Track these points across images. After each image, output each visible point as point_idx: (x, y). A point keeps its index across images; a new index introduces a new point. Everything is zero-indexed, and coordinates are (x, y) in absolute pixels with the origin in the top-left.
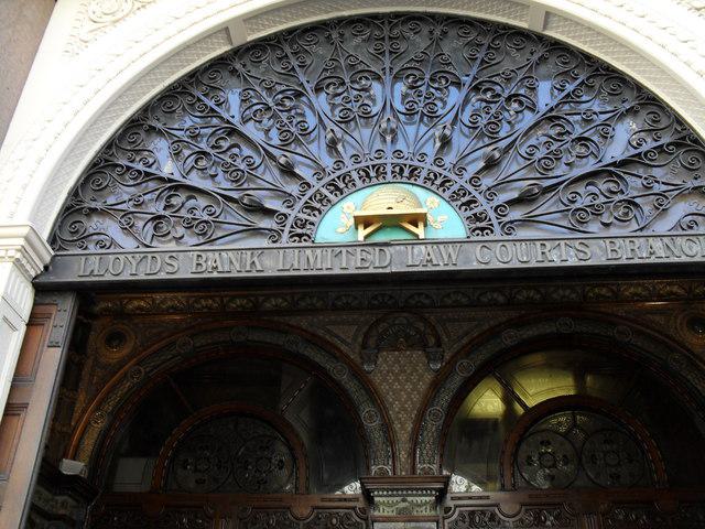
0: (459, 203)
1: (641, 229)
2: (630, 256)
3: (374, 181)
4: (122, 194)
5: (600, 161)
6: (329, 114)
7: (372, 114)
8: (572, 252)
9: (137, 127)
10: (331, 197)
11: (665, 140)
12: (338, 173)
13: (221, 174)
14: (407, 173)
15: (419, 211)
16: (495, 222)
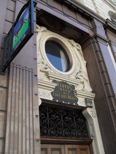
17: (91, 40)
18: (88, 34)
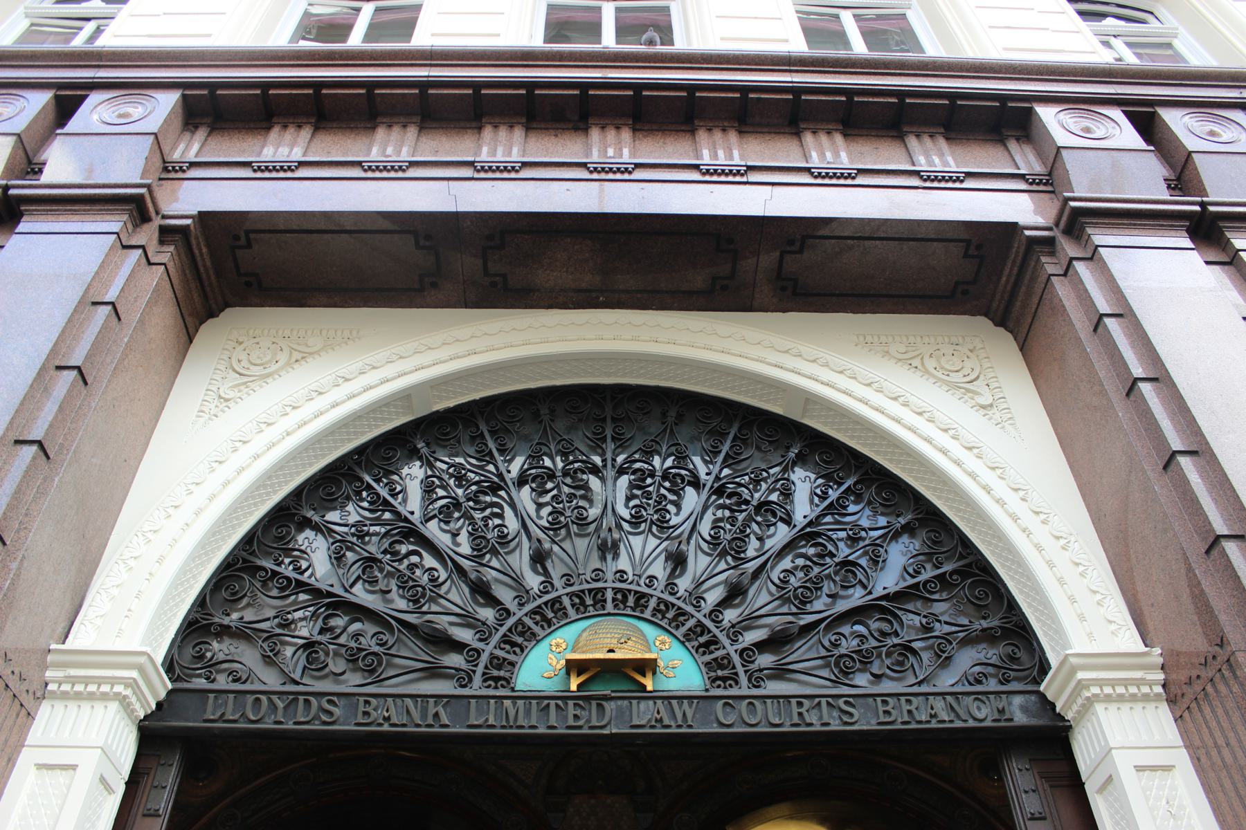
0: (696, 644)
1: (920, 683)
2: (906, 718)
3: (592, 611)
4: (259, 610)
5: (870, 593)
6: (533, 514)
7: (590, 519)
8: (835, 714)
9: (284, 520)
10: (536, 629)
11: (947, 567)
12: (546, 598)
13: (395, 588)
14: (632, 602)
15: (647, 656)
16: (740, 670)
17: (1044, 259)
18: (1010, 230)
